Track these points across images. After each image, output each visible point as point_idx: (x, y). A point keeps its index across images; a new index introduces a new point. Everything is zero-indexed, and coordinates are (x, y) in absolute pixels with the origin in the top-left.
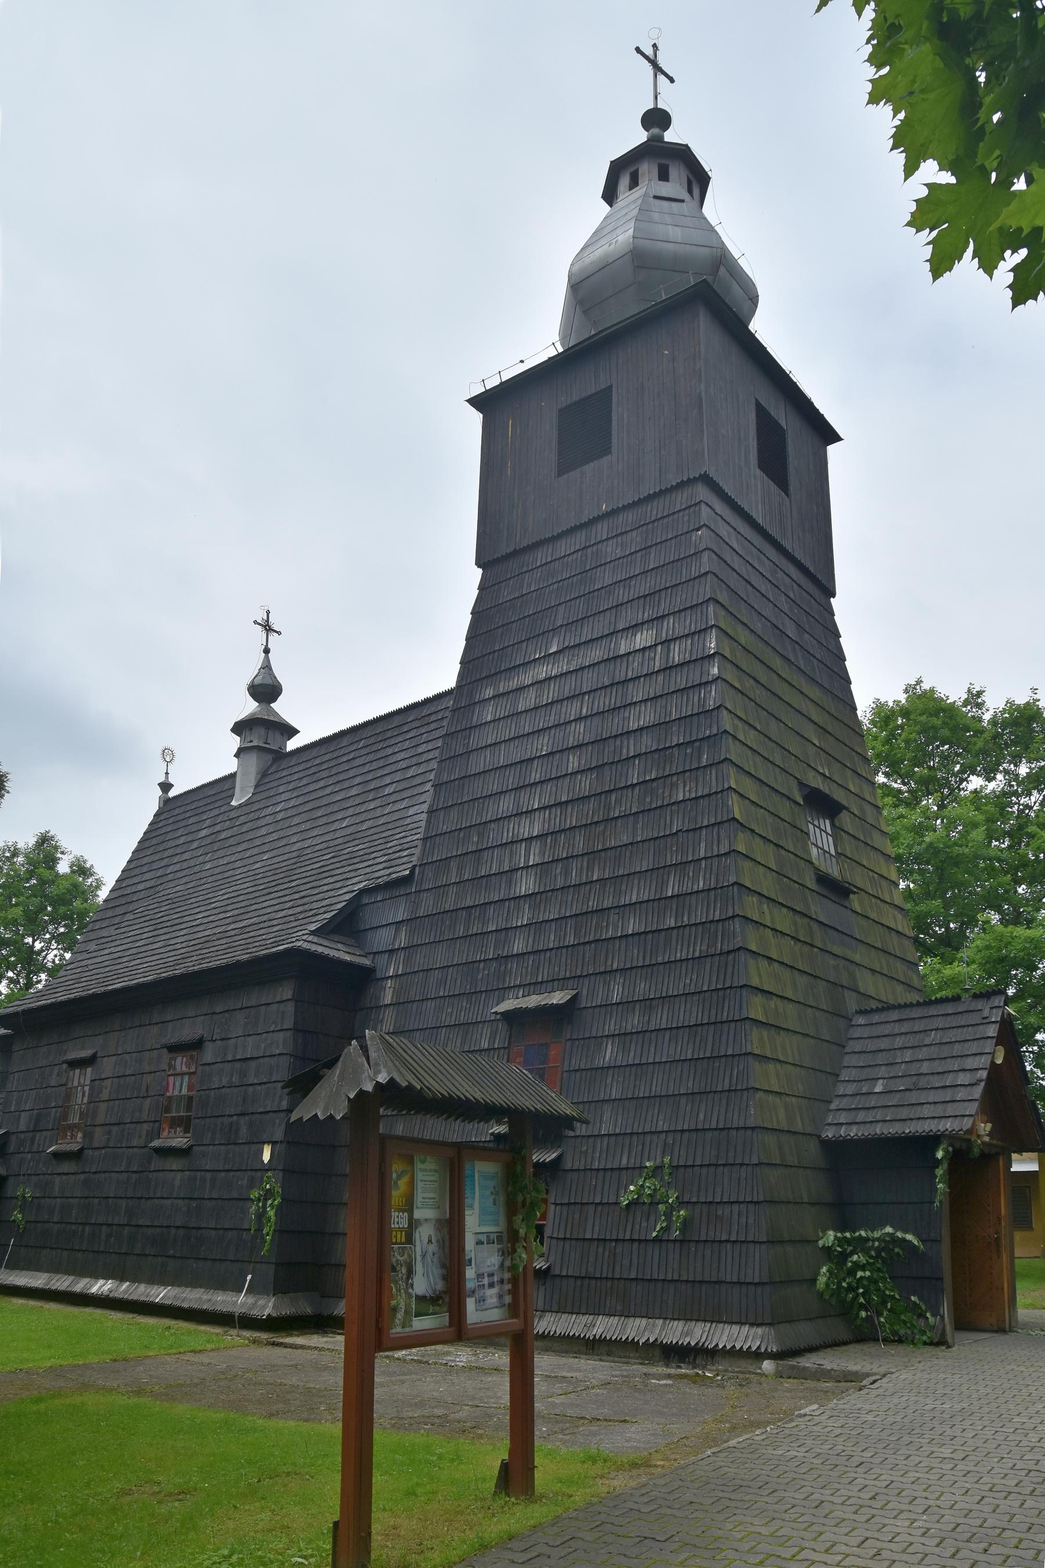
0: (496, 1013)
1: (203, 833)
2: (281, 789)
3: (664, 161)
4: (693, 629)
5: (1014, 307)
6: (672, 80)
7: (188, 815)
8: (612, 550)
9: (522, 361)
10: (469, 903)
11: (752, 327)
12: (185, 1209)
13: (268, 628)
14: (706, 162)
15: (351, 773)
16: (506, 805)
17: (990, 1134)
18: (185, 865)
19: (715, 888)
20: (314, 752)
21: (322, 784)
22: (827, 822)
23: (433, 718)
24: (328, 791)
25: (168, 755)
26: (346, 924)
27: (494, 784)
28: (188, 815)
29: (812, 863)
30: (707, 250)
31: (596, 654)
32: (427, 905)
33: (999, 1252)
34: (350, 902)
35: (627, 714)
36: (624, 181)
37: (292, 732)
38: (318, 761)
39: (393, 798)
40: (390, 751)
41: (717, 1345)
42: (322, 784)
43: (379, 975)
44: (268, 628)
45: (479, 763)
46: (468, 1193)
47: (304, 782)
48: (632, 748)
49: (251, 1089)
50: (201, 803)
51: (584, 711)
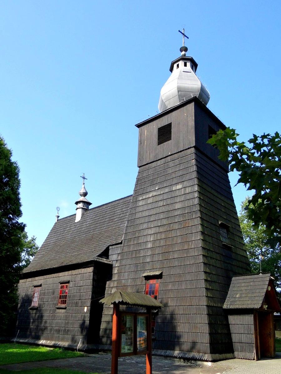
0: (143, 276)
1: (68, 229)
2: (88, 218)
3: (185, 61)
4: (191, 185)
5: (253, 134)
6: (188, 38)
7: (64, 224)
8: (171, 164)
9: (149, 116)
10: (136, 249)
11: (207, 106)
12: (64, 323)
13: (84, 178)
14: (197, 61)
15: (106, 215)
16: (145, 226)
17: (267, 308)
18: (63, 237)
19: (196, 248)
20: (97, 209)
21: (98, 217)
22: (225, 230)
23: (127, 202)
24: (100, 219)
25: (58, 209)
26: (106, 254)
27: (142, 221)
28: (64, 224)
29: (221, 240)
30: (196, 86)
31: (167, 190)
32: (126, 249)
33: (270, 337)
34: (107, 248)
35: (175, 205)
36: (175, 65)
37: (90, 204)
38: (97, 212)
39: (116, 222)
40: (115, 210)
41: (197, 358)
42: (98, 217)
43: (113, 266)
44: (84, 178)
45: (138, 215)
46: (138, 323)
47: (94, 217)
48: (176, 213)
49: (82, 293)
50: (67, 221)
51: (164, 204)
